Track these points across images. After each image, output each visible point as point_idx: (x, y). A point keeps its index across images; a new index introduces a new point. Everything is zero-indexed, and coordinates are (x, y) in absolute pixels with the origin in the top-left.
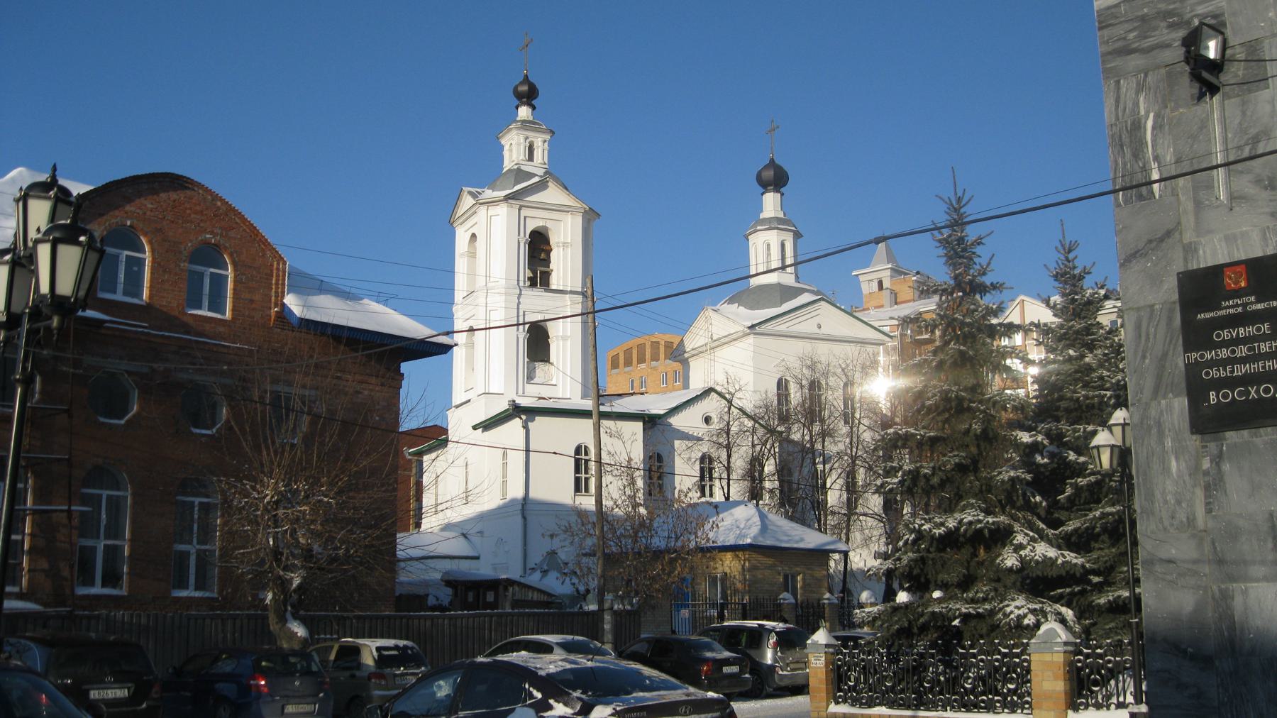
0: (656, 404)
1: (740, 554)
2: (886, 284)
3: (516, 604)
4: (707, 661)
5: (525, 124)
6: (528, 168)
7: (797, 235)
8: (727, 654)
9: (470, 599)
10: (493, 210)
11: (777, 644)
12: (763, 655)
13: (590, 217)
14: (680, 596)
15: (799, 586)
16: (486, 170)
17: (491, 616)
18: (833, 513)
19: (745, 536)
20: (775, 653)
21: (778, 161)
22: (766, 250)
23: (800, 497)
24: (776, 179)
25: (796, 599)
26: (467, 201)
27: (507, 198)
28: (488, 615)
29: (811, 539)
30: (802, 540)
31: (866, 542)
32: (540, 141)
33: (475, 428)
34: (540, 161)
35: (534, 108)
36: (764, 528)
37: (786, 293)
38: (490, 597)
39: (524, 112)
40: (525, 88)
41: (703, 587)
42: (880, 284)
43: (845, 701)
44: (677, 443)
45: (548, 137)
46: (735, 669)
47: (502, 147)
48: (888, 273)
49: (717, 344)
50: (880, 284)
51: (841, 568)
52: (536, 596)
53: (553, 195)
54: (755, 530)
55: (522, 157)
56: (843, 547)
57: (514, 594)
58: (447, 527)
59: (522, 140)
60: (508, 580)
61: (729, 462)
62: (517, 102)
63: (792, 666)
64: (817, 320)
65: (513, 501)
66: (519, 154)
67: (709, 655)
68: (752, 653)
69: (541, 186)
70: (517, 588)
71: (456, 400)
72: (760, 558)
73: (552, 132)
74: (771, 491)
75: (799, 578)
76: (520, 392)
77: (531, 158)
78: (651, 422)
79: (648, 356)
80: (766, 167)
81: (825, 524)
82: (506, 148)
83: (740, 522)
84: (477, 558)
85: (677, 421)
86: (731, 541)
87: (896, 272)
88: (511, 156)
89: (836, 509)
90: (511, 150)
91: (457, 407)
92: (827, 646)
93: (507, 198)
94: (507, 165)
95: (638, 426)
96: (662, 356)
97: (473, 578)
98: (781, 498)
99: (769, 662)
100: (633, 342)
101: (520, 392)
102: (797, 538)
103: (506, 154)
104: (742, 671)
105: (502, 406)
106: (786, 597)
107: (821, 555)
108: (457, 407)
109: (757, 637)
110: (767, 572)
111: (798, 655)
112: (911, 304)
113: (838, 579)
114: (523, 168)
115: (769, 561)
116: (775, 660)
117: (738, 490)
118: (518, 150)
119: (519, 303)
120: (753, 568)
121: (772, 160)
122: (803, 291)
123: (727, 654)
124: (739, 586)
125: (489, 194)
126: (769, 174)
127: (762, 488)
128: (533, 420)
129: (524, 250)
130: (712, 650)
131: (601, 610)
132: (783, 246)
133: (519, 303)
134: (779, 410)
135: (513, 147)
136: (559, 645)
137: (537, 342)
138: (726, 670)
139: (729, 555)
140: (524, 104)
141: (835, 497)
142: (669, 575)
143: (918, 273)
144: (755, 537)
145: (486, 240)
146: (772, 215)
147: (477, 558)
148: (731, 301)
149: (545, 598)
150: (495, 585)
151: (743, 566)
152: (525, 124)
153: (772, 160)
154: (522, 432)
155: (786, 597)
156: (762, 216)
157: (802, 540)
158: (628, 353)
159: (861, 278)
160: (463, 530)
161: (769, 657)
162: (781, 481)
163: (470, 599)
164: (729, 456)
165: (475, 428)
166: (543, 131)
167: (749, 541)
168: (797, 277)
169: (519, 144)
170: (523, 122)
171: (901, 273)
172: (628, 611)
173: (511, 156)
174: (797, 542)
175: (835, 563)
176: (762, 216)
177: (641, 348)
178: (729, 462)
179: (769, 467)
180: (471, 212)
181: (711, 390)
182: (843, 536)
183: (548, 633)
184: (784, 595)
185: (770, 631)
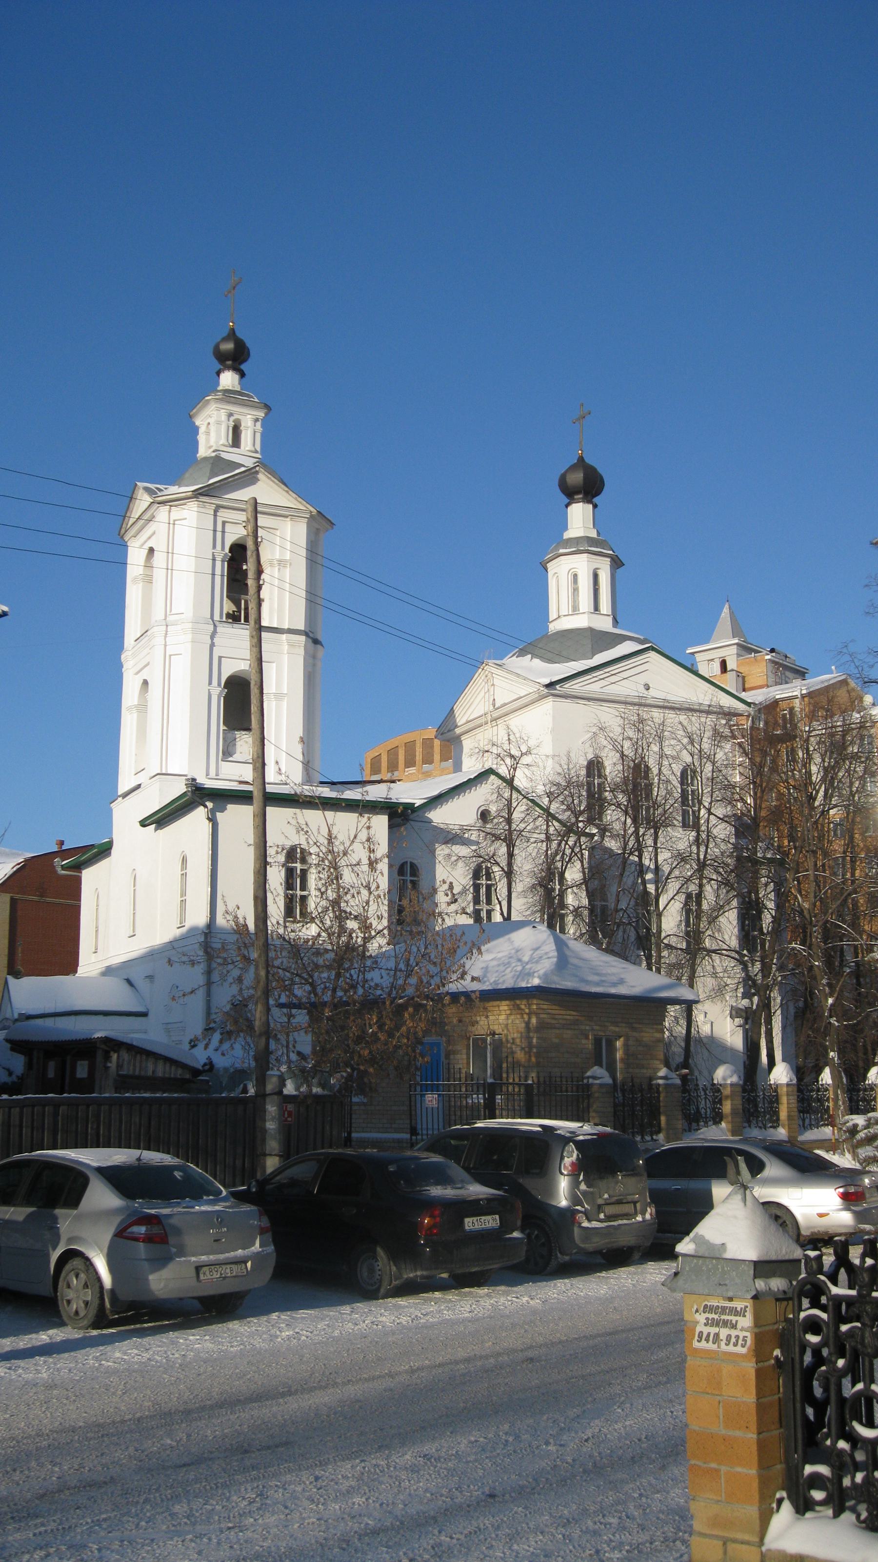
0: (410, 791)
1: (523, 1004)
2: (731, 665)
3: (124, 1082)
4: (430, 1204)
5: (229, 395)
6: (232, 455)
7: (617, 563)
8: (477, 1190)
9: (51, 1074)
10: (176, 513)
11: (578, 1168)
12: (551, 1189)
13: (320, 525)
14: (436, 1072)
15: (619, 1055)
16: (171, 458)
17: (56, 1105)
18: (669, 946)
19: (530, 974)
20: (575, 1184)
21: (589, 460)
22: (574, 594)
23: (619, 916)
24: (588, 486)
25: (614, 1079)
26: (143, 501)
27: (198, 494)
28: (50, 1101)
29: (636, 979)
30: (621, 982)
31: (719, 992)
32: (250, 421)
33: (144, 823)
34: (249, 447)
35: (242, 375)
36: (563, 961)
37: (600, 640)
38: (82, 1070)
39: (228, 379)
40: (229, 346)
41: (464, 1063)
42: (724, 664)
43: (839, 1502)
44: (441, 851)
45: (261, 414)
46: (490, 1222)
47: (195, 430)
48: (734, 650)
49: (498, 714)
50: (724, 664)
51: (681, 1030)
52: (161, 1070)
53: (267, 491)
54: (547, 965)
55: (223, 441)
56: (686, 993)
57: (119, 1066)
58: (109, 971)
59: (224, 417)
60: (107, 1040)
61: (510, 864)
62: (219, 366)
63: (611, 1210)
64: (642, 679)
65: (193, 930)
66: (218, 437)
67: (436, 1191)
68: (529, 1183)
69: (249, 477)
70: (125, 1055)
71: (122, 788)
72: (556, 1010)
73: (267, 407)
74: (577, 912)
75: (619, 1044)
76: (212, 773)
77: (236, 441)
78: (400, 816)
79: (419, 757)
80: (573, 468)
81: (658, 962)
82: (202, 430)
83: (521, 952)
84: (144, 1014)
85: (438, 816)
86: (507, 982)
87: (745, 649)
88: (208, 440)
89: (673, 941)
90: (208, 433)
91: (125, 795)
92: (763, 1268)
93: (198, 494)
94: (203, 451)
95: (381, 823)
96: (437, 757)
97: (55, 1038)
98: (592, 925)
99: (564, 1203)
100: (399, 740)
101: (212, 773)
102: (614, 979)
103: (201, 438)
104: (506, 1226)
105: (179, 788)
106: (598, 1074)
107: (651, 1007)
108: (125, 795)
109: (539, 1152)
110: (568, 1034)
111: (620, 1188)
112: (765, 690)
113: (678, 1050)
114: (224, 456)
115: (570, 1015)
116: (575, 1199)
117: (521, 906)
118: (218, 432)
119: (212, 645)
120: (542, 1026)
121: (581, 459)
122: (622, 639)
123: (477, 1190)
124: (520, 1056)
125: (174, 490)
126: (577, 478)
127: (562, 905)
128: (223, 810)
129: (221, 568)
130: (444, 1179)
131: (261, 1096)
132: (596, 576)
133: (212, 645)
134: (590, 785)
135: (211, 428)
136: (114, 1177)
137: (240, 702)
138: (471, 1224)
139: (504, 1006)
140: (228, 368)
141: (671, 921)
142: (391, 1035)
143: (772, 651)
144: (545, 977)
145: (170, 551)
146: (580, 533)
147: (144, 1014)
148: (522, 653)
149: (179, 1073)
150: (87, 1048)
151: (528, 1024)
152: (229, 395)
153: (581, 459)
154: (207, 826)
155: (598, 1074)
156: (567, 535)
157: (621, 982)
158: (393, 753)
159: (699, 657)
160: (123, 974)
161: (562, 1191)
162: (590, 895)
163: (51, 1074)
164: (511, 855)
165: (144, 823)
166: (253, 406)
167: (536, 982)
168: (616, 622)
169: (219, 423)
170: (226, 392)
171: (750, 650)
172: (317, 1097)
173: (208, 440)
174: (614, 985)
175: (673, 1022)
176: (567, 535)
177: (410, 747)
178: (510, 864)
179: (573, 874)
180: (147, 519)
181: (490, 772)
182: (684, 980)
183: (84, 1144)
184: (596, 1071)
185: (565, 1140)
